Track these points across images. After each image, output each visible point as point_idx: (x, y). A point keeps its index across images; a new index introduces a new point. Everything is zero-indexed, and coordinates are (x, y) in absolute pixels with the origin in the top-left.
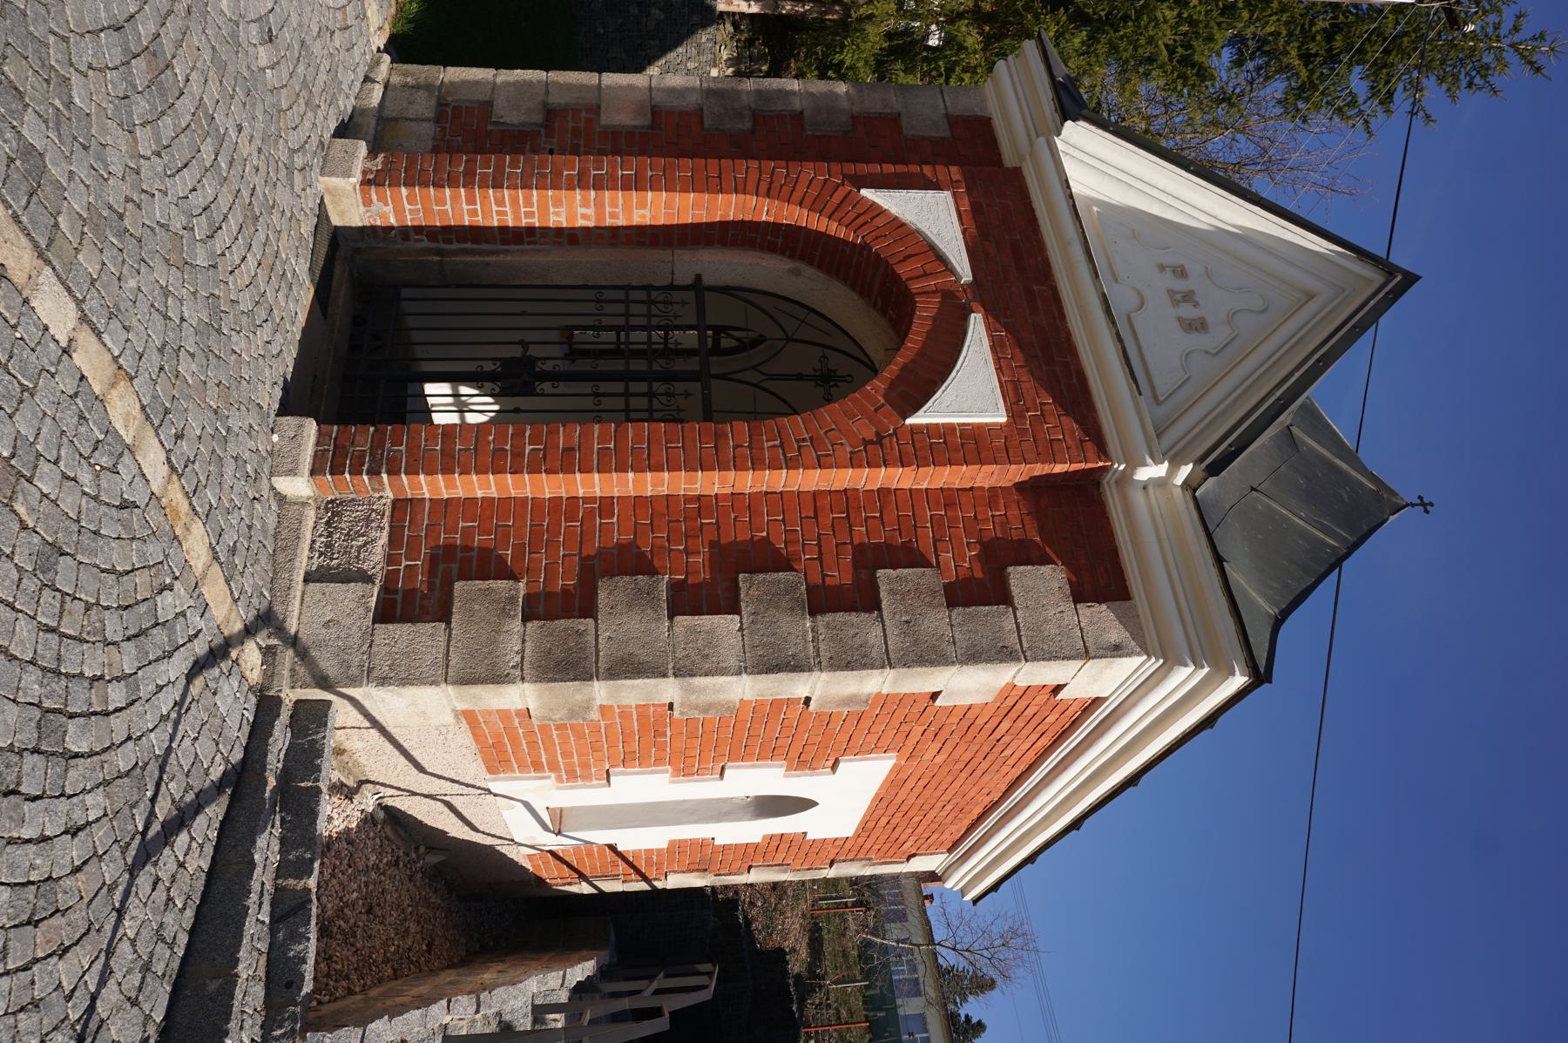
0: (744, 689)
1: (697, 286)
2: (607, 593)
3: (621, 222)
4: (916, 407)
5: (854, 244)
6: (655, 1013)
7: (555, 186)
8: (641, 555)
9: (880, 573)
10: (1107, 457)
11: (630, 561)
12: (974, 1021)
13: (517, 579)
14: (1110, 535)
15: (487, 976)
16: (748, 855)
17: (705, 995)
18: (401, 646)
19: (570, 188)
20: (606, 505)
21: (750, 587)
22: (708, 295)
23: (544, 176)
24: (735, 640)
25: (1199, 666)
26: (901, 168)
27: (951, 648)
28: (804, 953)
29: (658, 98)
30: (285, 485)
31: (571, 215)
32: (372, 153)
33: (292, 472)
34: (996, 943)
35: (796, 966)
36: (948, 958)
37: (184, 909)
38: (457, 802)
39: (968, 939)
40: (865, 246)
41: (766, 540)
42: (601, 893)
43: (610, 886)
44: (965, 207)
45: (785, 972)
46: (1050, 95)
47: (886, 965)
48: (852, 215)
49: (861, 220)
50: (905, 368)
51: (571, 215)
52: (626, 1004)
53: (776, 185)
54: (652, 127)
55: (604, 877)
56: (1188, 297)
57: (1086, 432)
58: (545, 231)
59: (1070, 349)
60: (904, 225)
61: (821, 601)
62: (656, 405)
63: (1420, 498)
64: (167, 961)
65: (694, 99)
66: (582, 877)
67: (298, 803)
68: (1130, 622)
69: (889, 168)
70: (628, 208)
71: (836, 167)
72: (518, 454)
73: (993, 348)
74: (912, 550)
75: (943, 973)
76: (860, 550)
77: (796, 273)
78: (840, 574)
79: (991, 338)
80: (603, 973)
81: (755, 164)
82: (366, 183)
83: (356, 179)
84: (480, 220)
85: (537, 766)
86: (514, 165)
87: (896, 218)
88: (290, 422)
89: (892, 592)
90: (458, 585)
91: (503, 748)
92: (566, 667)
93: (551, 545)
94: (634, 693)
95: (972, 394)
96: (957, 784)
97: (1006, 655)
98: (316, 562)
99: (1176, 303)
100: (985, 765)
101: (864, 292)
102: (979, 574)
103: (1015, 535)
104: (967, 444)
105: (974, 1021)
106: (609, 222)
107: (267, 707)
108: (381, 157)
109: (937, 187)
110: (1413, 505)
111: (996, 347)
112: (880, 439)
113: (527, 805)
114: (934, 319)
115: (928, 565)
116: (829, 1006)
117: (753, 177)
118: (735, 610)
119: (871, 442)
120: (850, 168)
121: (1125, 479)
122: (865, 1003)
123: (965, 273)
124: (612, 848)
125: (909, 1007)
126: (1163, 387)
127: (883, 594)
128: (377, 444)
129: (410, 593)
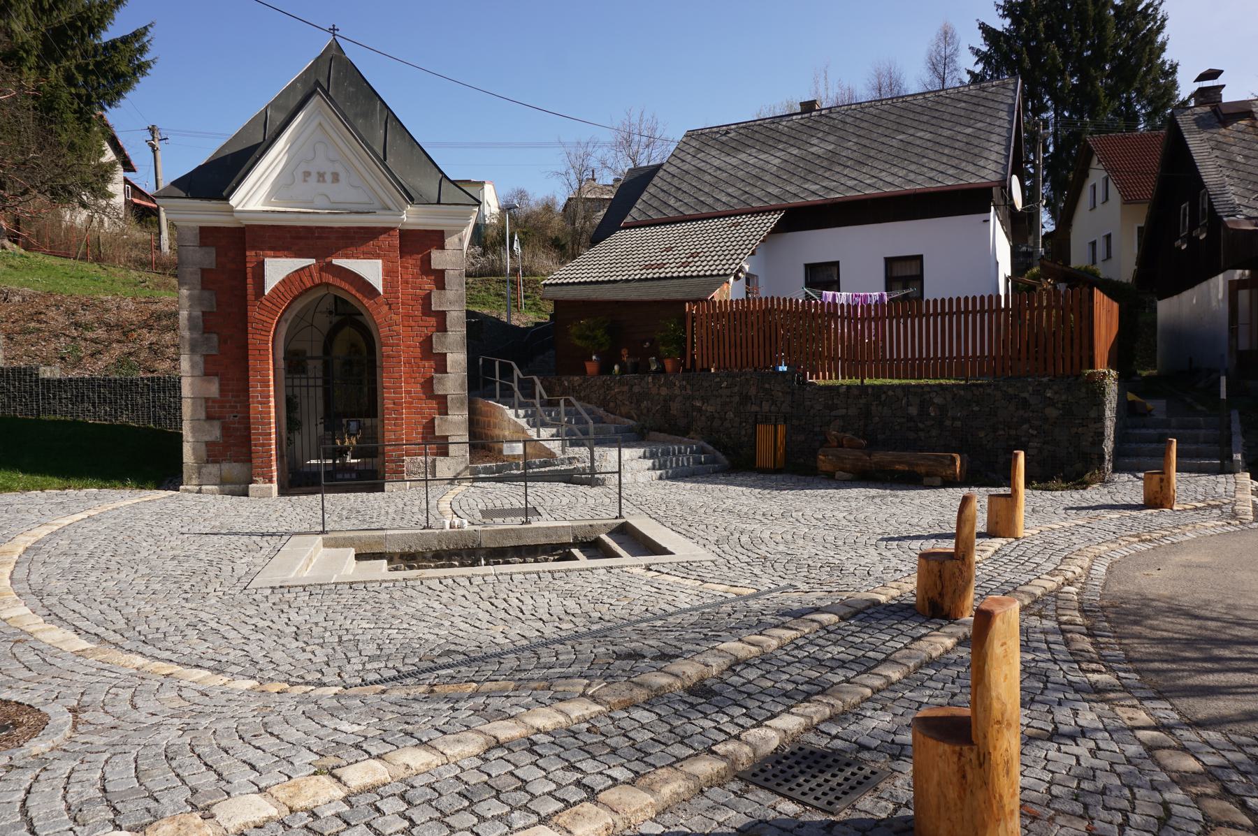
2: (439, 391)
4: (375, 290)
11: (428, 385)
21: (437, 349)
24: (455, 355)
29: (197, 373)
37: (411, 820)
65: (198, 358)
68: (452, 233)
71: (249, 303)
76: (424, 314)
78: (433, 321)
81: (250, 336)
95: (371, 270)
99: (324, 181)
104: (388, 273)
120: (250, 297)
123: (313, 261)
128: (393, 461)
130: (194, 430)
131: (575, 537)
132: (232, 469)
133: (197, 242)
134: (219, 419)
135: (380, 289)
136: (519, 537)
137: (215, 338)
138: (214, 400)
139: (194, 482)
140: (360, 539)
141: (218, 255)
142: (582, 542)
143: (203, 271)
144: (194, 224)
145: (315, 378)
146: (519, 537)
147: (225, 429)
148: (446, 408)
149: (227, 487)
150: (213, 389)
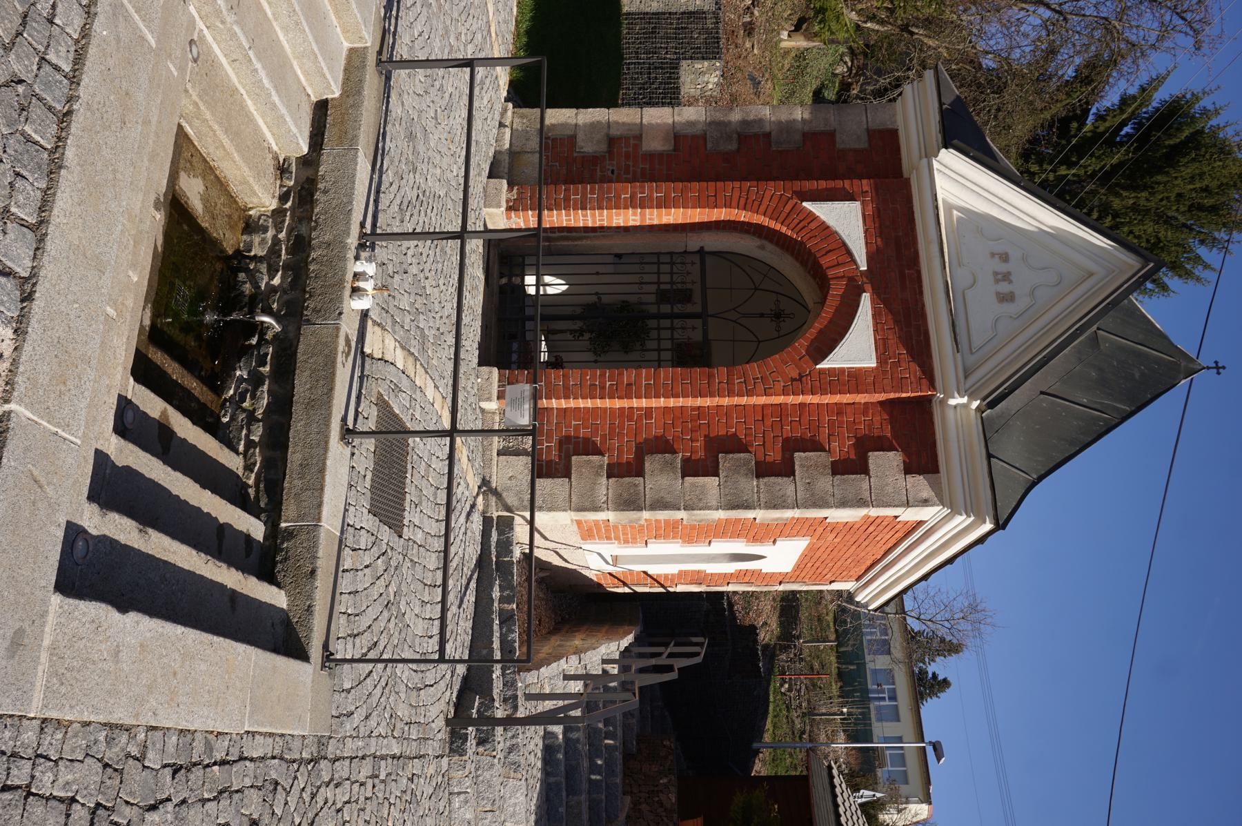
0: (721, 514)
1: (701, 252)
2: (650, 463)
3: (656, 222)
4: (824, 356)
5: (796, 240)
6: (669, 669)
7: (618, 207)
8: (667, 441)
9: (796, 454)
10: (934, 389)
11: (662, 446)
12: (940, 678)
13: (603, 455)
14: (933, 434)
15: (577, 642)
16: (727, 578)
17: (698, 660)
18: (547, 490)
19: (626, 208)
20: (649, 411)
22: (709, 260)
23: (609, 199)
25: (969, 516)
26: (831, 184)
27: (831, 499)
28: (774, 624)
30: (485, 405)
31: (626, 220)
32: (511, 185)
33: (489, 399)
34: (956, 616)
35: (764, 636)
36: (915, 625)
38: (561, 552)
39: (932, 611)
40: (802, 243)
41: (735, 434)
42: (635, 592)
43: (639, 589)
44: (869, 212)
45: (755, 641)
46: (938, 118)
47: (858, 628)
48: (796, 221)
49: (801, 225)
50: (820, 332)
51: (626, 220)
52: (653, 662)
53: (750, 201)
54: (675, 150)
55: (638, 585)
56: (1006, 277)
57: (924, 372)
58: (609, 228)
59: (923, 316)
60: (828, 227)
61: (763, 470)
62: (675, 270)
63: (1216, 362)
64: (467, 643)
66: (625, 584)
67: (504, 568)
69: (823, 184)
70: (660, 216)
71: (788, 184)
72: (603, 387)
73: (874, 316)
74: (815, 441)
75: (911, 637)
76: (786, 441)
77: (762, 247)
78: (774, 455)
79: (874, 308)
80: (638, 641)
81: (737, 184)
82: (509, 209)
83: (503, 209)
84: (572, 224)
85: (609, 538)
86: (592, 192)
87: (824, 222)
88: (485, 369)
89: (802, 466)
90: (574, 458)
91: (588, 533)
92: (629, 503)
93: (620, 435)
94: (663, 515)
95: (857, 349)
96: (851, 550)
97: (861, 503)
98: (502, 444)
99: (997, 281)
100: (866, 543)
101: (803, 263)
102: (853, 456)
103: (876, 433)
104: (853, 379)
105: (940, 678)
106: (648, 222)
107: (487, 521)
108: (515, 191)
109: (850, 197)
110: (1208, 368)
111: (876, 316)
112: (801, 376)
113: (599, 554)
114: (841, 296)
115: (824, 450)
116: (801, 660)
117: (736, 194)
118: (717, 475)
119: (795, 380)
120: (797, 185)
121: (943, 402)
122: (838, 657)
124: (645, 573)
125: (876, 663)
126: (977, 341)
127: (797, 467)
129: (549, 462)
130: (594, 126)
131: (290, 534)
132: (531, 165)
133: (873, 126)
134: (610, 152)
135: (824, 365)
136: (310, 405)
137: (733, 146)
138: (636, 147)
139: (517, 120)
140: (357, 106)
141: (856, 151)
142: (277, 549)
143: (831, 135)
144: (899, 118)
145: (672, 273)
146: (310, 405)
147: (594, 160)
148: (621, 476)
149: (506, 159)
150: (653, 144)
